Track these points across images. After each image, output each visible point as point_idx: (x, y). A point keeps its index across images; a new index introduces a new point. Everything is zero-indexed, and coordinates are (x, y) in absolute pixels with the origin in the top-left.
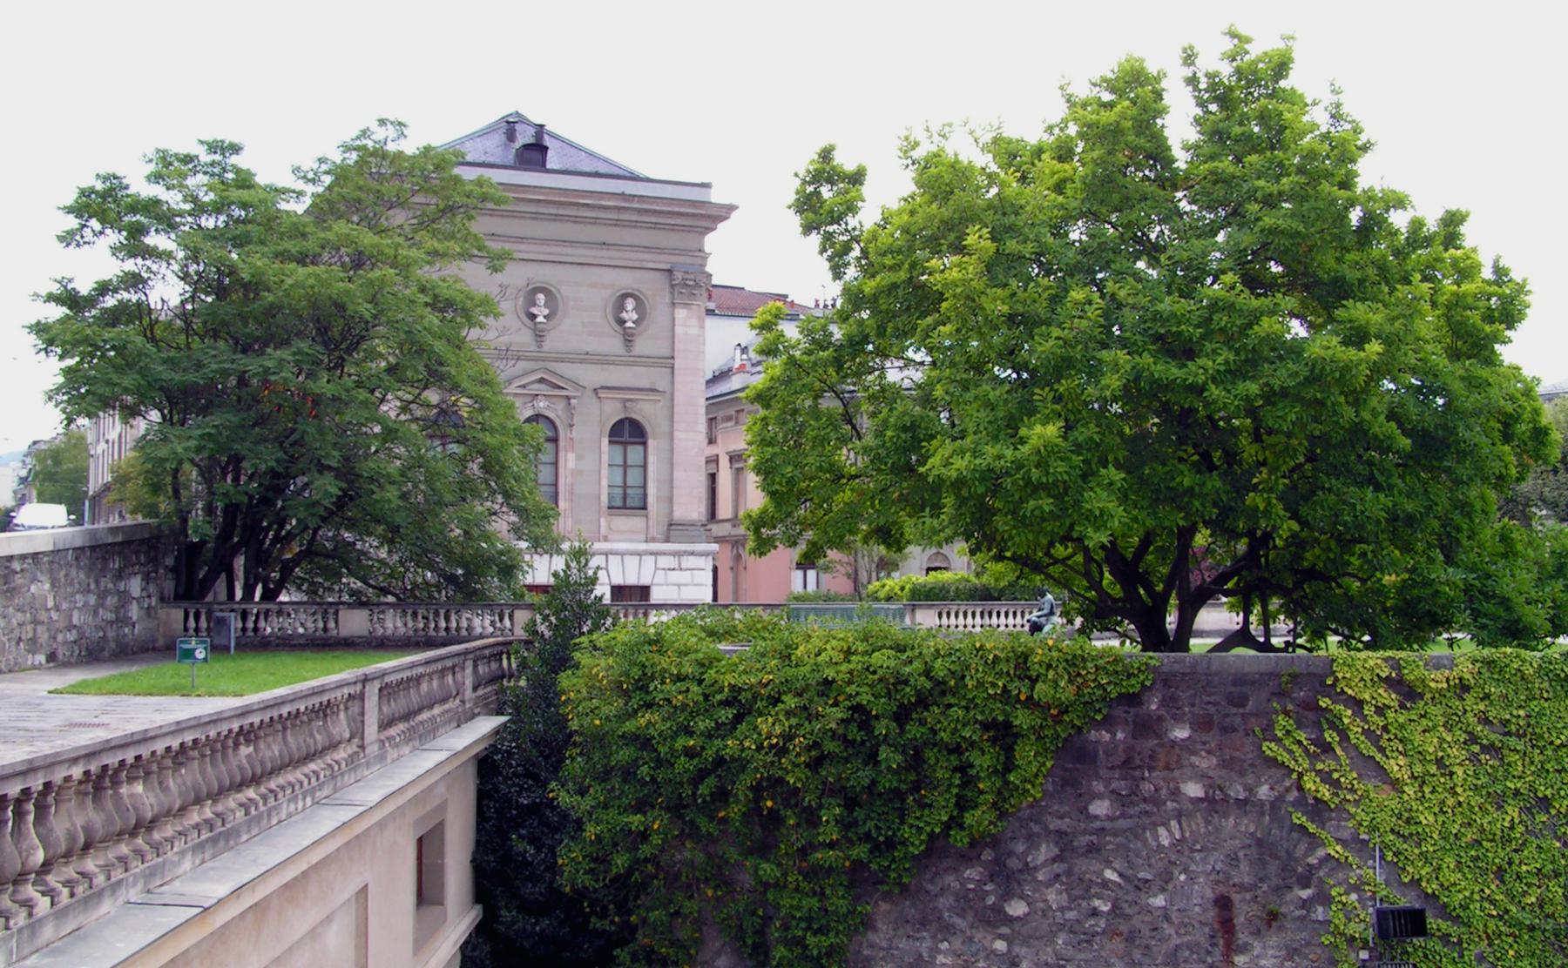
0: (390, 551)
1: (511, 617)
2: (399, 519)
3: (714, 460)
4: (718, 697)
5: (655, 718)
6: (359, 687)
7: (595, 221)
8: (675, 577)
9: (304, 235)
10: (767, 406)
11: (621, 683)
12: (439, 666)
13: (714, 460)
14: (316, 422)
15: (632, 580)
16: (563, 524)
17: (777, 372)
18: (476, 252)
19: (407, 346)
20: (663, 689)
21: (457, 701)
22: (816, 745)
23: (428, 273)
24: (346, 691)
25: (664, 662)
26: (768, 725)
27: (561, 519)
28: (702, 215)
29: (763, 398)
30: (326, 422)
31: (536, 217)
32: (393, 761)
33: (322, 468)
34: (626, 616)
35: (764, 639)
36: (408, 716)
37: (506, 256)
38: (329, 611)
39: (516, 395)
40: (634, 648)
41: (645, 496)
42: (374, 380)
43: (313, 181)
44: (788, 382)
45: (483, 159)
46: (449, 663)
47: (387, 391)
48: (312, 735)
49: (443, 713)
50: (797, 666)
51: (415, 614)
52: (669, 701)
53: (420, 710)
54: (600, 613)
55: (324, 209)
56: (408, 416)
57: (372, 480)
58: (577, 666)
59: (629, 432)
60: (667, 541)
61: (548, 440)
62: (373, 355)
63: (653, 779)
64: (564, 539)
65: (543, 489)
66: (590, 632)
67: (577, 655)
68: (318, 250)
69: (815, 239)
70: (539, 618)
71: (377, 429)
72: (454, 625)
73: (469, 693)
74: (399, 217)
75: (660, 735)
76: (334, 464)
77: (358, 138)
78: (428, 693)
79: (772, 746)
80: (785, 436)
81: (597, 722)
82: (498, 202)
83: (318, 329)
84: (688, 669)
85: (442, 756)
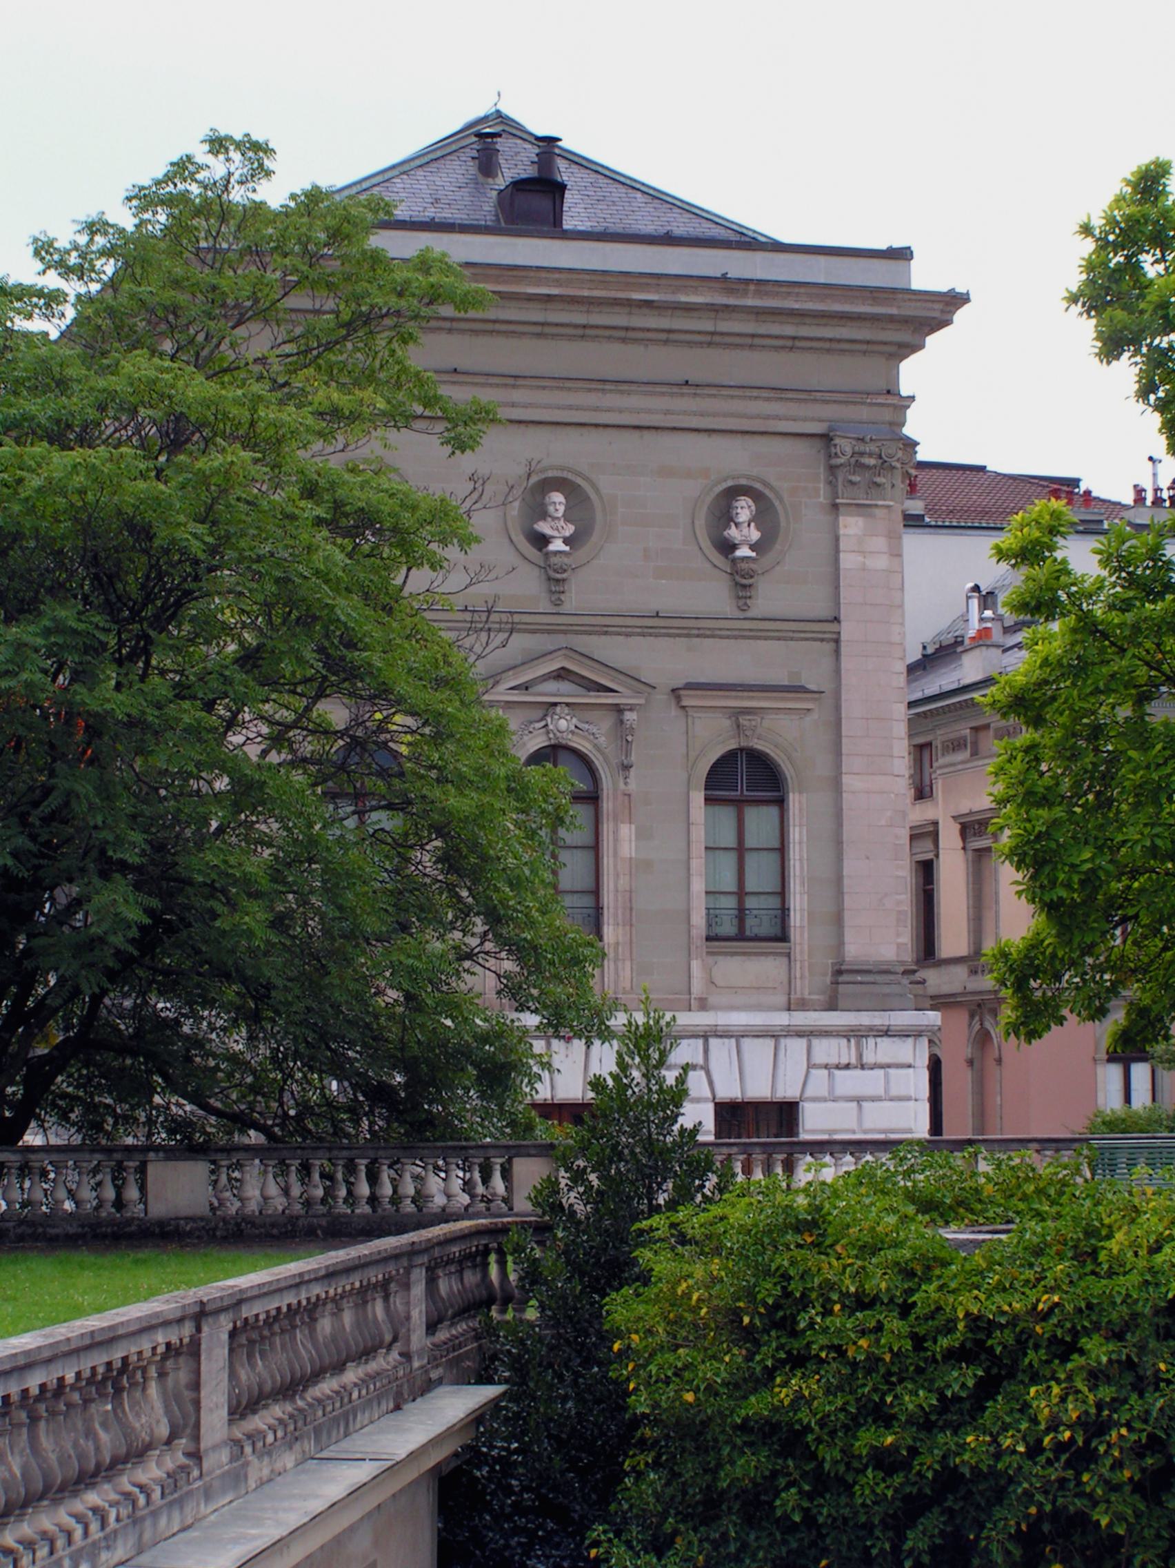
0: (251, 1038)
1: (506, 1174)
2: (271, 970)
3: (927, 833)
4: (944, 1342)
5: (811, 1386)
6: (187, 1330)
7: (668, 338)
8: (849, 1082)
9: (62, 385)
10: (1037, 722)
11: (737, 1314)
12: (356, 1280)
13: (927, 833)
14: (93, 772)
15: (759, 1090)
16: (615, 976)
17: (1056, 648)
18: (419, 409)
19: (279, 611)
20: (824, 1326)
21: (394, 1355)
22: (1155, 1444)
23: (322, 457)
24: (161, 1338)
25: (829, 1268)
26: (1051, 1402)
27: (609, 965)
28: (891, 319)
29: (1027, 704)
30: (119, 771)
31: (542, 331)
32: (262, 1483)
33: (109, 868)
34: (747, 1170)
35: (1040, 1216)
36: (289, 1389)
37: (484, 416)
38: (126, 1165)
39: (509, 705)
40: (765, 1238)
41: (784, 912)
42: (214, 683)
43: (80, 272)
44: (1078, 669)
45: (430, 213)
46: (376, 1275)
47: (241, 702)
48: (90, 1433)
49: (363, 1382)
50: (1111, 1274)
51: (305, 1170)
52: (840, 1351)
53: (317, 1375)
54: (690, 1165)
55: (103, 328)
56: (285, 756)
57: (212, 890)
58: (645, 1278)
59: (746, 778)
60: (832, 1006)
61: (578, 798)
62: (209, 629)
63: (809, 1519)
64: (616, 1005)
65: (568, 901)
66: (672, 1205)
67: (644, 1255)
68: (92, 414)
69: (1127, 370)
70: (564, 1178)
71: (222, 784)
72: (387, 1190)
73: (418, 1338)
74: (257, 341)
75: (822, 1423)
76: (133, 858)
77: (168, 178)
78: (334, 1338)
79: (1060, 1447)
80: (1077, 784)
81: (689, 1397)
82: (464, 302)
83: (96, 577)
84: (879, 1283)
85: (362, 1473)
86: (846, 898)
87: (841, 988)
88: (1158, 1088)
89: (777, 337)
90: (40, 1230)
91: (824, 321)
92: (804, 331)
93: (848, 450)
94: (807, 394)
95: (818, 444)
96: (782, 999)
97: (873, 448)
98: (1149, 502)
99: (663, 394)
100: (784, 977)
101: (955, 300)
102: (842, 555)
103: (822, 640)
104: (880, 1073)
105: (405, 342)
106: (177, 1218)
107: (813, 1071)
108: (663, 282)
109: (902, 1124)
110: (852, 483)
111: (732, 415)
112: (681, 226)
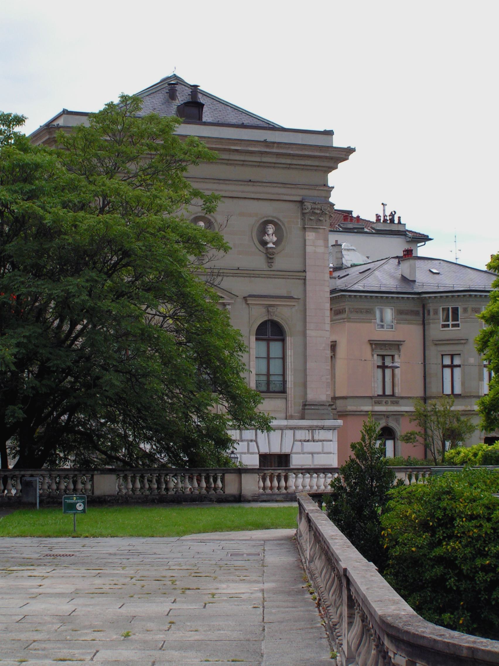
5: (457, 545)
7: (243, 164)
8: (309, 447)
15: (276, 449)
25: (460, 507)
28: (326, 158)
41: (284, 382)
60: (303, 418)
84: (480, 511)
86: (308, 376)
87: (306, 411)
88: (397, 450)
89: (284, 164)
90: (55, 500)
91: (301, 158)
92: (294, 162)
93: (310, 207)
94: (294, 186)
95: (298, 204)
96: (283, 415)
97: (319, 206)
98: (382, 221)
99: (241, 185)
100: (284, 407)
101: (350, 151)
102: (307, 247)
103: (299, 279)
104: (320, 443)
105: (182, 171)
106: (104, 496)
107: (295, 443)
108: (243, 142)
109: (329, 463)
110: (311, 219)
111: (269, 193)
112: (247, 121)
